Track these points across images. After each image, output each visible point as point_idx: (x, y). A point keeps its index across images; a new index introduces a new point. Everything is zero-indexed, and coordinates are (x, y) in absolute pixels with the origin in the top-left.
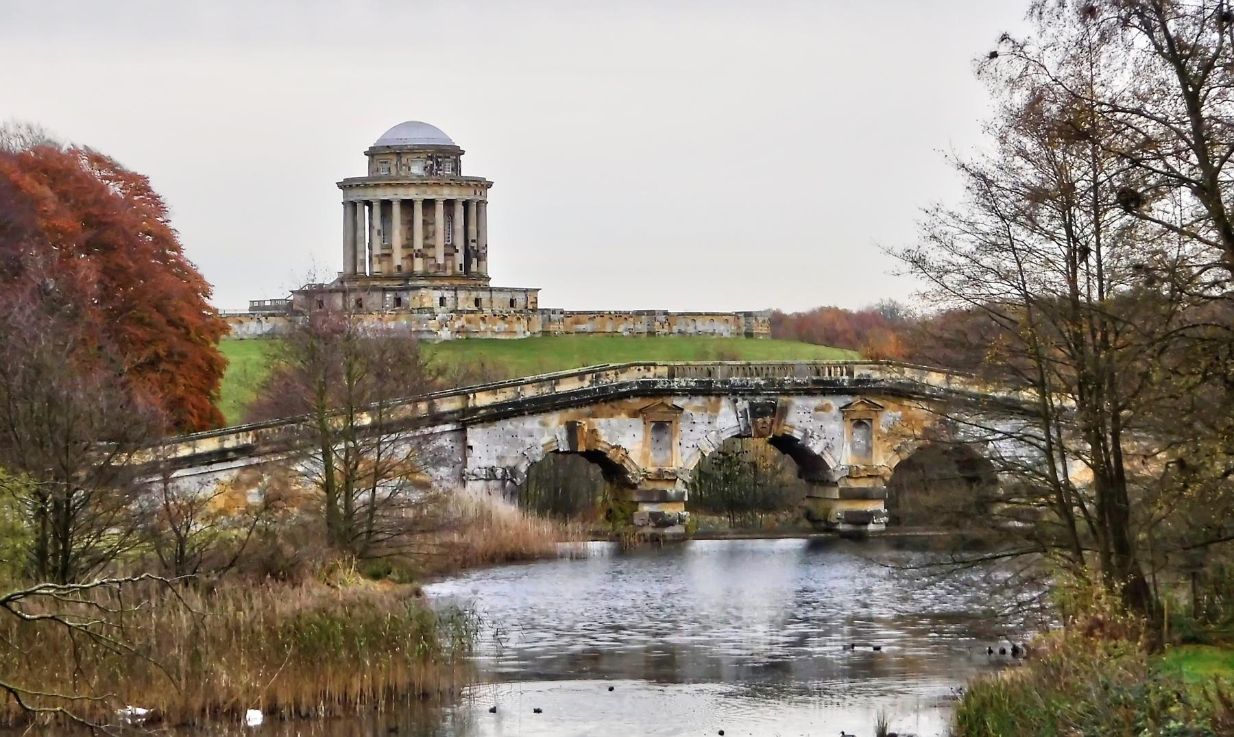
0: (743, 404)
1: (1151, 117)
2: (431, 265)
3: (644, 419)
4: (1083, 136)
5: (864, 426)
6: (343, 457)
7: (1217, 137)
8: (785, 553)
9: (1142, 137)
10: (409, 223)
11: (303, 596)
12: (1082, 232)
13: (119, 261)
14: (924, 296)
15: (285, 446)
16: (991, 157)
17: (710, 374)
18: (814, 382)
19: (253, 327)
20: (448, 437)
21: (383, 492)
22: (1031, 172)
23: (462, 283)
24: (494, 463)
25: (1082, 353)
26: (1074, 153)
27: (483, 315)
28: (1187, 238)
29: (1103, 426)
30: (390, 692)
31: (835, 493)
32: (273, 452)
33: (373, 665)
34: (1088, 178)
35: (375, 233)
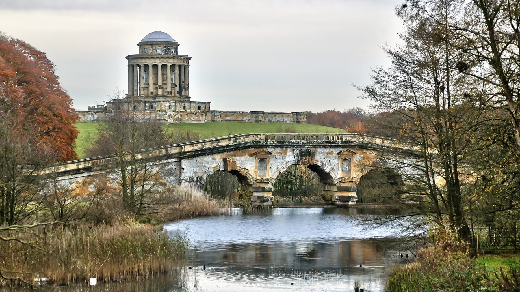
0: (297, 151)
1: (471, 32)
2: (165, 92)
3: (256, 157)
4: (443, 39)
5: (347, 161)
6: (130, 172)
7: (500, 40)
8: (313, 215)
9: (468, 40)
10: (156, 74)
11: (115, 231)
12: (441, 80)
13: (32, 88)
14: (374, 107)
15: (105, 167)
16: (403, 49)
17: (283, 139)
18: (327, 142)
19: (90, 117)
20: (173, 164)
21: (147, 187)
22: (420, 55)
23: (178, 99)
24: (193, 175)
25: (441, 131)
26: (438, 47)
27: (187, 113)
28: (486, 83)
29: (450, 162)
30: (151, 270)
31: (335, 189)
32: (101, 170)
33: (144, 259)
34: (444, 58)
35: (142, 78)
